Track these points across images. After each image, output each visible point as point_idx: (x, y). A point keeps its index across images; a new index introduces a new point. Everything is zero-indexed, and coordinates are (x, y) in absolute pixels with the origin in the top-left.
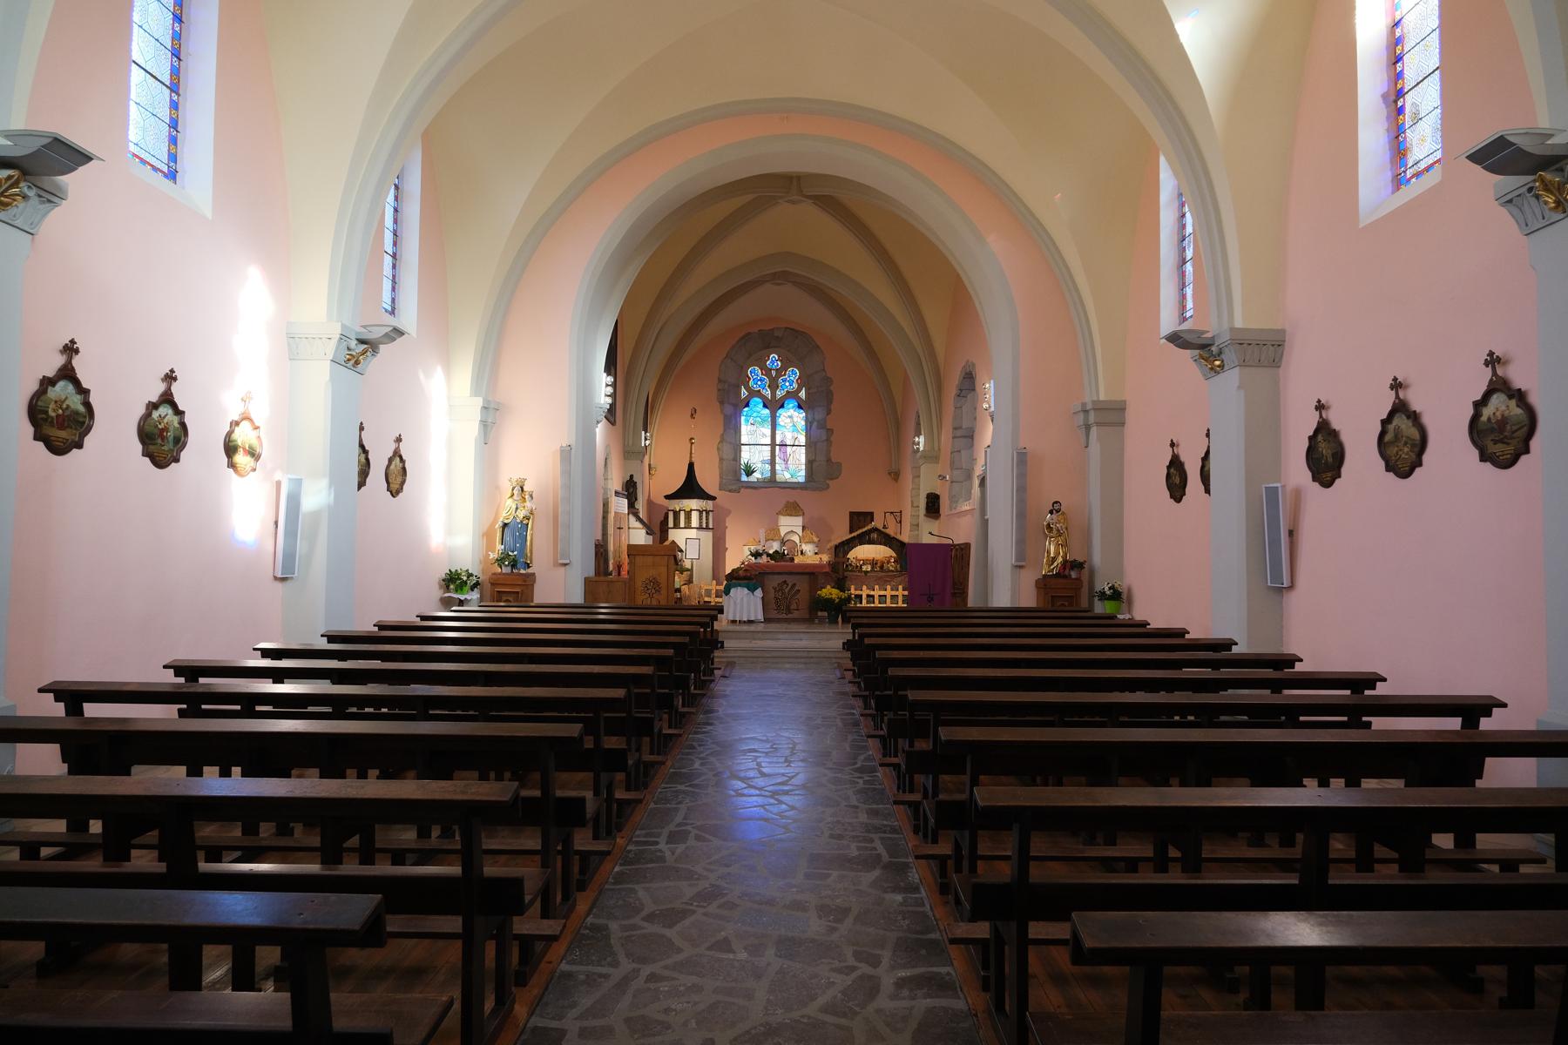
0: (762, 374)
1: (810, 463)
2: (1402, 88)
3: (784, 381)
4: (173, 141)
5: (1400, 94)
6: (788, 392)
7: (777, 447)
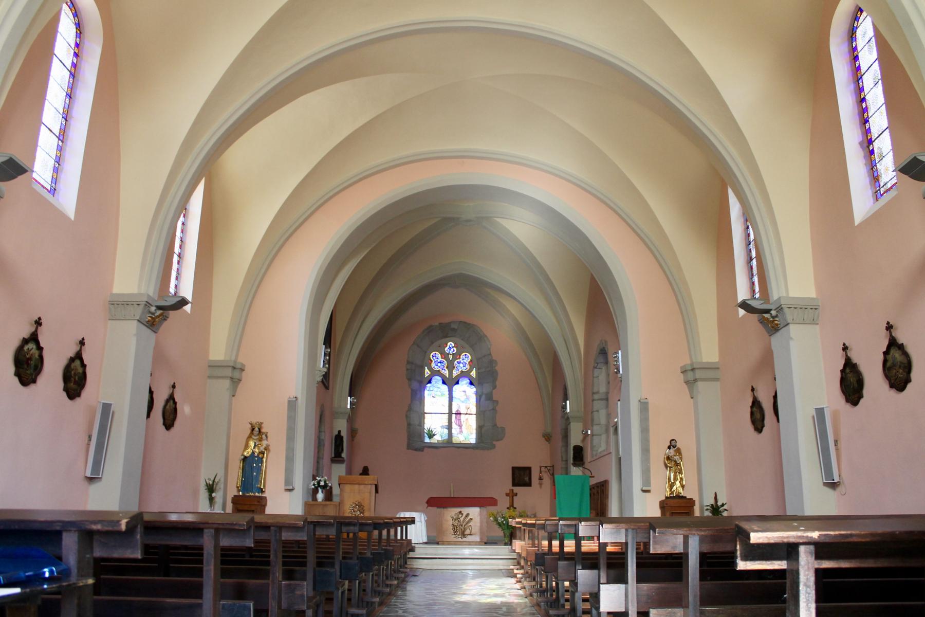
0: (442, 358)
1: (480, 429)
2: (871, 138)
3: (459, 363)
4: (56, 170)
5: (870, 142)
6: (462, 372)
7: (454, 416)
